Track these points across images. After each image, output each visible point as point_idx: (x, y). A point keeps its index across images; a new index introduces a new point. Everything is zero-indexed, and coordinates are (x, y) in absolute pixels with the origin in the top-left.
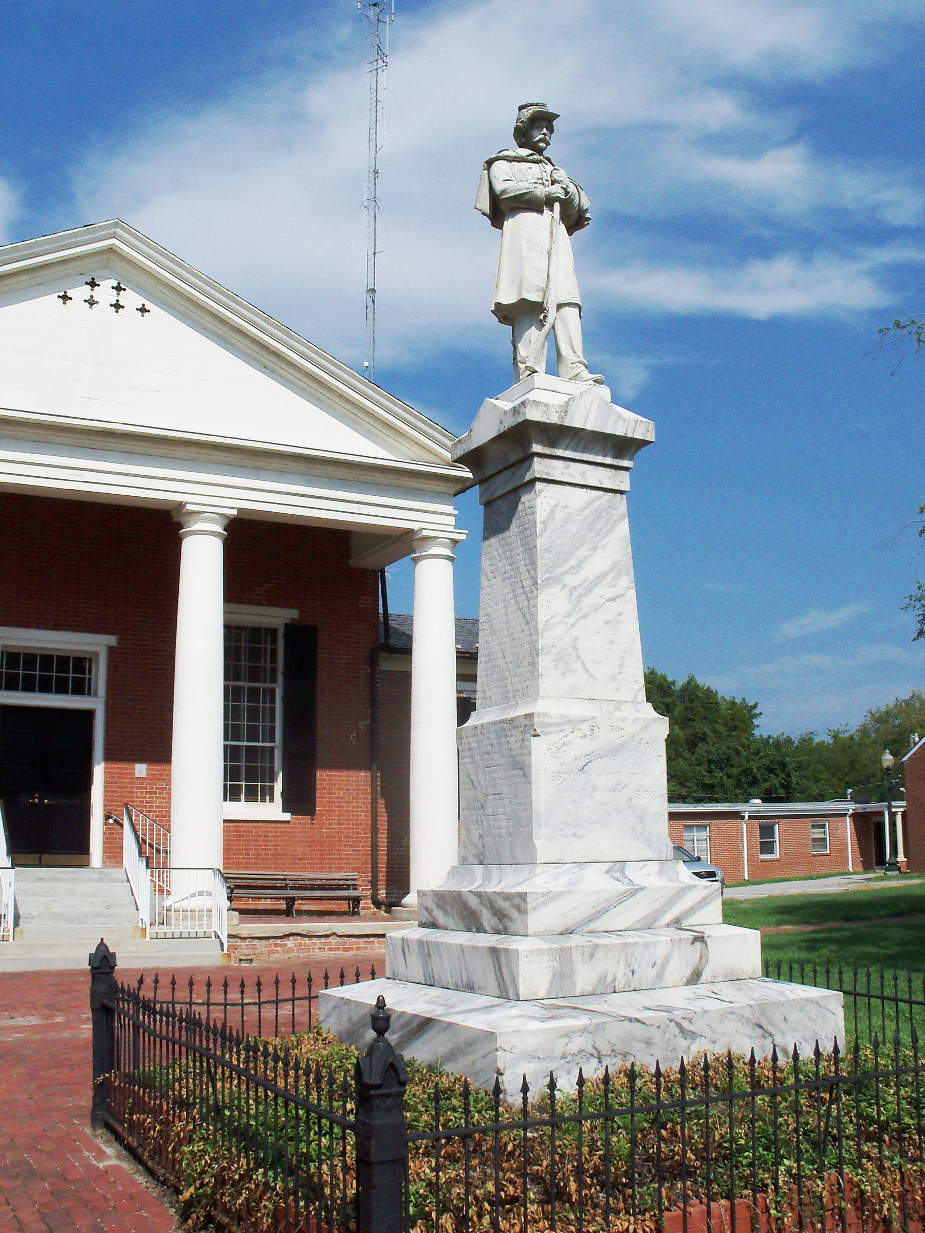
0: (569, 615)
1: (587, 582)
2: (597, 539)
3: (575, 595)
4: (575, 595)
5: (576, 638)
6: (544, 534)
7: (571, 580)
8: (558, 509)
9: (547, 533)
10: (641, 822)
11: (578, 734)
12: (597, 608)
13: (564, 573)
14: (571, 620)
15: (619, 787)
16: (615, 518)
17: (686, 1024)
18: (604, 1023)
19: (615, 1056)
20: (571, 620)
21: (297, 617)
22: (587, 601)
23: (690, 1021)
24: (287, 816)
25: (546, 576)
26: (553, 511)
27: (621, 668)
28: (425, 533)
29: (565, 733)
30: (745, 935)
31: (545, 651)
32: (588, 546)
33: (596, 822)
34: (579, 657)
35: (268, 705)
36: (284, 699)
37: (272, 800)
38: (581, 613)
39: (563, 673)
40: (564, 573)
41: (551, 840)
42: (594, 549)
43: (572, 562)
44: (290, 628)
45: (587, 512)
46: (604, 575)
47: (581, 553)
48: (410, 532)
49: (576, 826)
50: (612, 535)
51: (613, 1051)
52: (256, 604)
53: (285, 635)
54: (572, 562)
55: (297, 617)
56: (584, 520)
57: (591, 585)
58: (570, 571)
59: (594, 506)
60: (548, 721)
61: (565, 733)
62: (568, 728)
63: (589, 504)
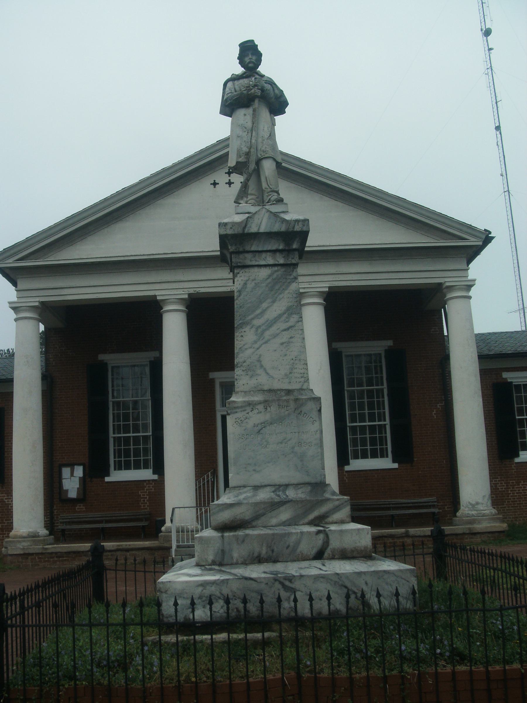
0: (255, 342)
1: (269, 322)
2: (276, 295)
3: (260, 330)
4: (260, 330)
5: (260, 356)
6: (239, 298)
7: (257, 322)
8: (249, 282)
9: (241, 297)
10: (302, 461)
11: (256, 411)
12: (275, 336)
13: (253, 319)
14: (256, 346)
15: (285, 441)
16: (288, 281)
17: (287, 583)
18: (228, 579)
19: (235, 599)
20: (256, 346)
21: (392, 344)
22: (267, 334)
23: (290, 581)
24: (396, 466)
25: (240, 322)
26: (245, 284)
27: (292, 369)
28: (447, 284)
29: (247, 412)
30: (359, 530)
31: (239, 365)
32: (269, 300)
33: (269, 462)
34: (262, 366)
35: (381, 399)
36: (388, 395)
37: (387, 457)
38: (264, 341)
39: (251, 377)
40: (253, 319)
41: (238, 474)
42: (274, 302)
43: (258, 311)
44: (389, 352)
45: (269, 280)
46: (280, 316)
47: (265, 305)
48: (440, 284)
49: (255, 465)
50: (287, 292)
51: (234, 596)
52: (366, 340)
53: (385, 357)
54: (258, 311)
55: (392, 344)
56: (267, 286)
57: (271, 324)
58: (257, 317)
59: (275, 276)
60: (236, 405)
61: (247, 412)
62: (249, 409)
63: (270, 276)
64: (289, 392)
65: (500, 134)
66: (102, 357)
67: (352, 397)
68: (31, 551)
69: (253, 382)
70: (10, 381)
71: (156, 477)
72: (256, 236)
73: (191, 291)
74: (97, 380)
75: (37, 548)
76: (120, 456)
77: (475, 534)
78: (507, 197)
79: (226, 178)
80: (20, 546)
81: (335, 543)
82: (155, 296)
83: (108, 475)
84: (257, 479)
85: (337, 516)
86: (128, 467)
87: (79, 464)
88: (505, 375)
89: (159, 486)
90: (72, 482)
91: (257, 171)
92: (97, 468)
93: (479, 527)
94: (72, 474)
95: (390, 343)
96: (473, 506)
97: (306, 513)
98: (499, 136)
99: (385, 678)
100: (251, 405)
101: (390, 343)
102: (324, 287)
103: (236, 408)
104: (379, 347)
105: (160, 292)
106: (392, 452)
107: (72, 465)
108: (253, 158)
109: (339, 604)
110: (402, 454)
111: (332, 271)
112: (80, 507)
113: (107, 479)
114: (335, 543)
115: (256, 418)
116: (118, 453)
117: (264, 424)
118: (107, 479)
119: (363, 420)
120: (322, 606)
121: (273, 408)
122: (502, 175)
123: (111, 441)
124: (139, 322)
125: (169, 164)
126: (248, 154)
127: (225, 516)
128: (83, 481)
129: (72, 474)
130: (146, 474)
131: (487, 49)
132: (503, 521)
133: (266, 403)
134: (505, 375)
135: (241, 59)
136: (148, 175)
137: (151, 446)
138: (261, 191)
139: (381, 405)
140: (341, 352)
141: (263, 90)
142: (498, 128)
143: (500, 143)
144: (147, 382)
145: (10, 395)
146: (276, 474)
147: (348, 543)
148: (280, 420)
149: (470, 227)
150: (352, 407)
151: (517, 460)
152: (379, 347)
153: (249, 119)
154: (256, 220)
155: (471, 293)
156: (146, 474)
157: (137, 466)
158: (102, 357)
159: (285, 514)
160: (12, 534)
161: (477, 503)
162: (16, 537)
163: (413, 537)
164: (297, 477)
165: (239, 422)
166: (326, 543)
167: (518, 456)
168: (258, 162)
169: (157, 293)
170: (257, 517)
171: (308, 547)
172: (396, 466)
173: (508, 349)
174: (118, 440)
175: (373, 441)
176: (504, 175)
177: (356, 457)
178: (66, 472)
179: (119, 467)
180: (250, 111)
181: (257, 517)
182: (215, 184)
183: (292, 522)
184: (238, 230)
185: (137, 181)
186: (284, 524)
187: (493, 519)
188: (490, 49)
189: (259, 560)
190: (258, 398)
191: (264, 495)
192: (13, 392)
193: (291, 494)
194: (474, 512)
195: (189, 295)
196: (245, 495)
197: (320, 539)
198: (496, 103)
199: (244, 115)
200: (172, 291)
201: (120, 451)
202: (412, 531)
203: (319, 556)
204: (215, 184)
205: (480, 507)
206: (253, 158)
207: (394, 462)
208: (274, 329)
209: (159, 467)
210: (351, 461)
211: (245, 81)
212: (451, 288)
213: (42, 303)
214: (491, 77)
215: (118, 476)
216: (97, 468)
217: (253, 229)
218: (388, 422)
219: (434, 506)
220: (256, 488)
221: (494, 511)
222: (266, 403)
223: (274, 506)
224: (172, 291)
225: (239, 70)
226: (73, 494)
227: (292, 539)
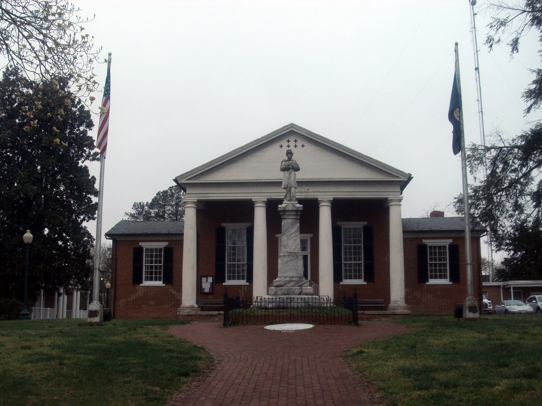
24: (365, 283)
48: (387, 198)
64: (295, 253)
65: (479, 72)
66: (223, 225)
67: (345, 249)
68: (190, 314)
69: (286, 250)
70: (183, 234)
71: (248, 284)
72: (288, 211)
73: (269, 197)
74: (220, 236)
75: (194, 313)
76: (230, 273)
77: (395, 315)
78: (481, 116)
79: (287, 144)
80: (186, 311)
81: (304, 291)
82: (251, 199)
83: (224, 282)
84: (285, 275)
85: (305, 285)
86: (234, 278)
87: (211, 276)
88: (424, 241)
89: (250, 288)
90: (207, 285)
91: (290, 191)
92: (219, 278)
93: (397, 312)
94: (207, 281)
95: (366, 223)
96: (395, 302)
97: (298, 283)
98: (477, 74)
99: (309, 316)
100: (285, 256)
101: (366, 223)
102: (331, 198)
103: (281, 257)
104: (360, 225)
105: (254, 198)
106: (364, 277)
107: (207, 277)
108: (289, 187)
109: (303, 305)
110: (369, 277)
111: (336, 190)
112: (210, 297)
113: (224, 284)
114: (304, 291)
115: (286, 259)
116: (229, 271)
117: (288, 261)
118: (224, 284)
119: (350, 260)
120: (300, 305)
121: (291, 257)
122: (478, 101)
123: (226, 265)
124: (243, 211)
125: (260, 137)
126: (287, 185)
127: (277, 284)
128: (212, 284)
129: (207, 281)
130: (243, 282)
131: (472, 14)
132: (409, 309)
133: (289, 256)
134: (424, 241)
135: (287, 154)
136: (250, 142)
137: (246, 268)
138: (291, 197)
139: (359, 253)
140: (341, 227)
141: (292, 166)
142: (477, 69)
143: (478, 79)
144: (245, 238)
145: (182, 241)
146: (291, 274)
147: (307, 291)
148: (292, 260)
149: (402, 172)
150: (346, 253)
151: (427, 283)
152: (360, 225)
153: (288, 174)
154: (288, 206)
155: (401, 203)
156: (243, 282)
157: (239, 278)
158: (223, 225)
159: (292, 284)
160: (182, 306)
161: (398, 301)
162: (184, 307)
163: (366, 314)
164: (296, 275)
165: (281, 260)
166: (302, 291)
167: (428, 281)
168: (290, 188)
169: (252, 198)
170: (285, 284)
171: (297, 292)
172: (365, 283)
173: (421, 228)
174: (229, 266)
175: (355, 271)
176: (480, 101)
177: (346, 278)
178: (204, 279)
179: (230, 278)
180: (289, 172)
181: (285, 284)
182: (281, 146)
183: (294, 286)
184: (283, 209)
185: (244, 144)
186: (293, 286)
187: (404, 308)
188: (475, 14)
189: (285, 294)
190: (287, 254)
191: (287, 279)
192: (183, 240)
193: (294, 279)
194: (396, 305)
195: (268, 199)
196: (283, 279)
197: (300, 290)
198: (477, 51)
199: (287, 173)
200: (259, 197)
201: (230, 270)
202: (366, 312)
203: (300, 294)
204: (281, 146)
205: (399, 303)
206: (289, 187)
207: (365, 281)
208: (292, 236)
209: (250, 279)
210: (343, 280)
211: (288, 162)
212: (391, 200)
213: (198, 200)
214: (474, 34)
215: (228, 283)
216: (219, 278)
217: (287, 209)
218: (363, 262)
219: (383, 304)
220: (285, 277)
221: (405, 305)
222: (289, 256)
223: (289, 282)
224: (259, 197)
225: (286, 158)
226: (207, 291)
227: (293, 290)
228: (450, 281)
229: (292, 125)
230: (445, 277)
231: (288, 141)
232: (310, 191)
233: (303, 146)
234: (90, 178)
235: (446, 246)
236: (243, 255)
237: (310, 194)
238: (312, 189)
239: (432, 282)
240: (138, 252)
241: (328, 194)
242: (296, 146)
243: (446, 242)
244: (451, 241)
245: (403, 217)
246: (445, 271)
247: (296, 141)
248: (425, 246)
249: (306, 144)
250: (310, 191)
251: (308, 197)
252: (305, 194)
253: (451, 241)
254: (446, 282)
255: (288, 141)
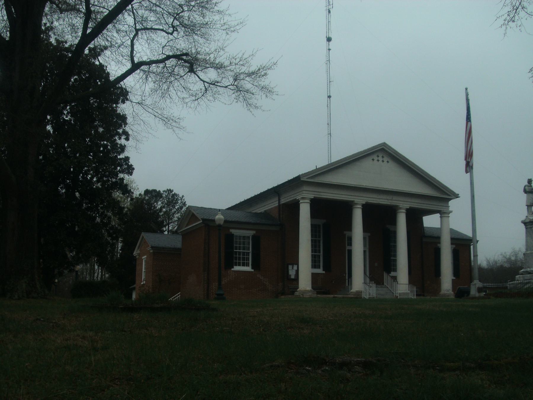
48: (398, 206)
102: (408, 206)
151: (232, 269)
172: (324, 272)
182: (373, 160)
228: (323, 270)
229: (384, 144)
230: (248, 265)
231: (378, 156)
232: (394, 199)
233: (388, 162)
234: (122, 156)
235: (249, 237)
236: (320, 247)
237: (394, 202)
238: (395, 198)
239: (237, 268)
240: (230, 238)
241: (359, 198)
242: (383, 161)
243: (250, 233)
244: (254, 232)
245: (451, 227)
246: (248, 259)
247: (383, 157)
248: (232, 235)
249: (390, 161)
250: (394, 199)
251: (392, 204)
252: (390, 201)
253: (254, 232)
254: (248, 269)
255: (378, 156)
